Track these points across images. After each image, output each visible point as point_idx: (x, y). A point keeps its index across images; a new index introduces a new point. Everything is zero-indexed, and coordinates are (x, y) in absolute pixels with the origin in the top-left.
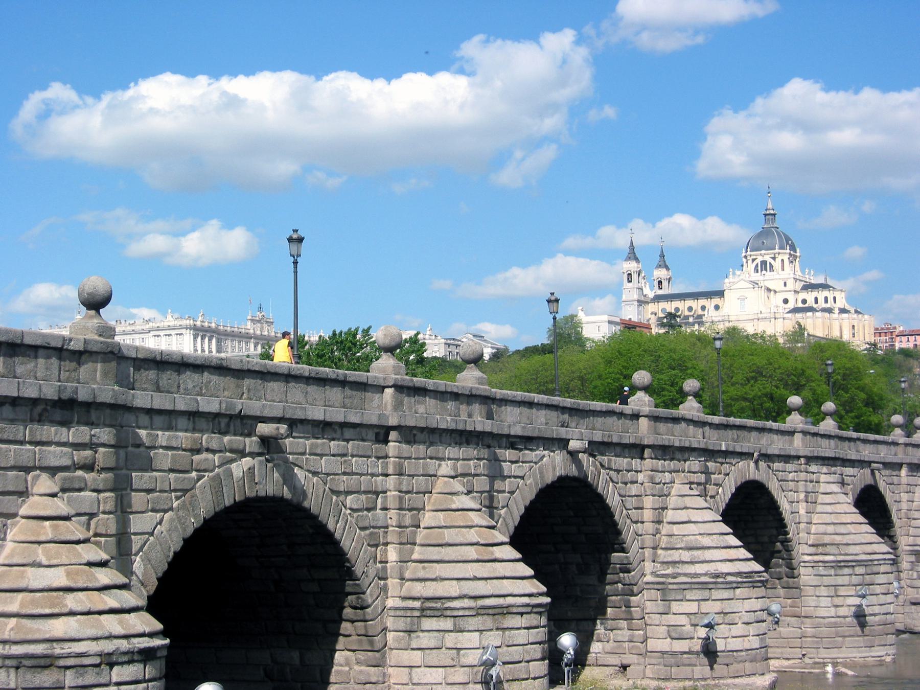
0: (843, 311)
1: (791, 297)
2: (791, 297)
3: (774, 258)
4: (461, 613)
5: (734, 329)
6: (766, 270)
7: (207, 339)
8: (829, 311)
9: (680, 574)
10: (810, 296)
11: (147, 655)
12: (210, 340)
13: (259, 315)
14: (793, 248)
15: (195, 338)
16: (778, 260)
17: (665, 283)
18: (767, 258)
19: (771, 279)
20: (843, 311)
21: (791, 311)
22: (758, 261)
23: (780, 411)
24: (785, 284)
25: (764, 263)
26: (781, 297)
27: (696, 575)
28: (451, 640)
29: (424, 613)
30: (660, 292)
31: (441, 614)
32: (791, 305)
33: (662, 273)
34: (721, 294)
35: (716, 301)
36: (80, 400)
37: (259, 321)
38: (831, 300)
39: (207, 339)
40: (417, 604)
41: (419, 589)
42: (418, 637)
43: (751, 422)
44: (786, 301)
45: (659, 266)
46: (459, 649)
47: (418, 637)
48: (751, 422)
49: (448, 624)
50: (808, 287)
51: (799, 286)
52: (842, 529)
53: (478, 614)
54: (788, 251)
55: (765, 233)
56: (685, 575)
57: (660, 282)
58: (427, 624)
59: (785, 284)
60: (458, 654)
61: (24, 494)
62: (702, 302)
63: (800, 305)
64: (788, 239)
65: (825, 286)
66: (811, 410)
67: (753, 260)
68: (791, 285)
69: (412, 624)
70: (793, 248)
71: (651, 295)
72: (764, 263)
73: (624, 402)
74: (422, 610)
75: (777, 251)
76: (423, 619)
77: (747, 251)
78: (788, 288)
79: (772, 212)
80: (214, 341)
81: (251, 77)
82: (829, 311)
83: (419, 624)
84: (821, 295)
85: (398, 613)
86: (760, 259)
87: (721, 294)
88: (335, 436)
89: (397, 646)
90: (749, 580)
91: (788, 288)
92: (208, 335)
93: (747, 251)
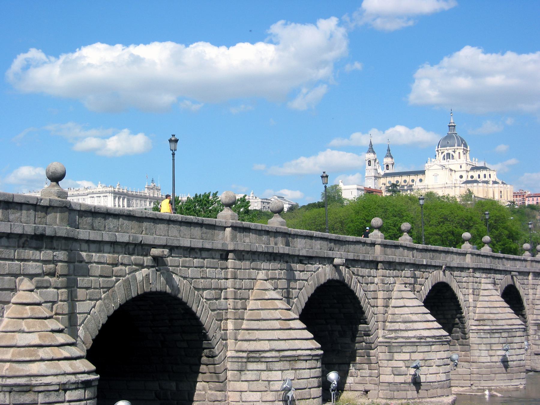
0: (495, 182)
1: (464, 174)
2: (464, 174)
3: (454, 152)
4: (270, 360)
5: (431, 193)
6: (450, 158)
7: (121, 199)
8: (487, 182)
9: (399, 337)
10: (475, 174)
11: (86, 385)
12: (123, 200)
13: (152, 185)
14: (465, 145)
15: (115, 198)
16: (457, 153)
17: (390, 166)
18: (450, 152)
19: (453, 164)
20: (495, 182)
21: (464, 183)
22: (445, 153)
23: (458, 241)
24: (461, 167)
25: (448, 154)
26: (458, 174)
27: (409, 338)
28: (265, 375)
29: (249, 360)
30: (387, 172)
31: (259, 360)
32: (464, 179)
33: (388, 160)
34: (423, 172)
35: (420, 176)
36: (47, 235)
37: (152, 189)
38: (487, 176)
39: (121, 199)
40: (245, 355)
41: (246, 346)
42: (245, 374)
43: (441, 248)
44: (461, 177)
45: (387, 156)
46: (269, 381)
47: (245, 374)
48: (441, 248)
49: (263, 366)
50: (475, 168)
51: (469, 168)
52: (494, 310)
53: (281, 361)
54: (463, 147)
55: (449, 137)
56: (402, 337)
57: (387, 166)
58: (251, 366)
59: (461, 167)
60: (269, 384)
61: (14, 290)
62: (412, 177)
63: (470, 179)
64: (462, 140)
65: (484, 168)
66: (476, 241)
67: (442, 153)
68: (464, 167)
69: (242, 366)
70: (465, 145)
71: (382, 173)
72: (448, 154)
73: (367, 236)
74: (248, 358)
75: (456, 147)
76: (249, 364)
77: (438, 148)
78: (462, 169)
79: (453, 124)
80: (126, 200)
81: (147, 45)
82: (487, 182)
83: (246, 366)
84: (482, 173)
85: (234, 360)
86: (446, 152)
87: (423, 172)
88: (196, 256)
89: (233, 379)
90: (439, 340)
91: (462, 169)
92: (122, 196)
93: (438, 148)
